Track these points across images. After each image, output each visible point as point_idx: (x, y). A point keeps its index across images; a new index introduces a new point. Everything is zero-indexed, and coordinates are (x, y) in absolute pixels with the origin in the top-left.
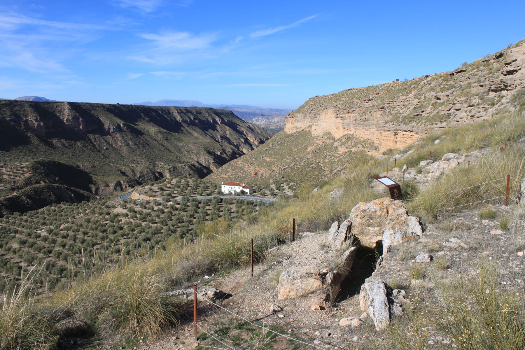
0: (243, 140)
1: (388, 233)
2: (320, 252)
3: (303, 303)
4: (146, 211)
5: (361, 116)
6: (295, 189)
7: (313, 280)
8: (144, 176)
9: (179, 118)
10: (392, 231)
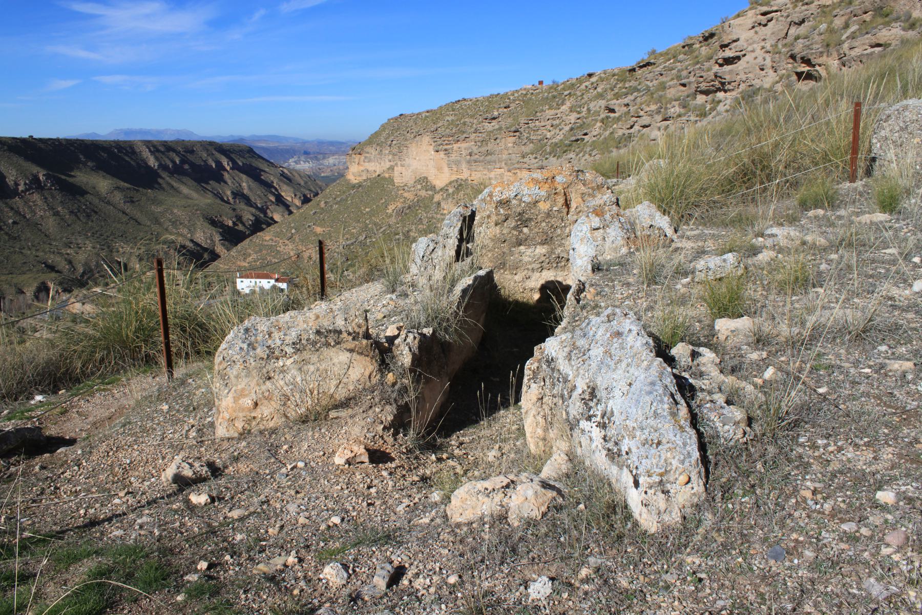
0: (273, 198)
1: (585, 228)
3: (307, 444)
5: (480, 147)
7: (344, 357)
8: (91, 271)
9: (152, 162)
10: (596, 222)
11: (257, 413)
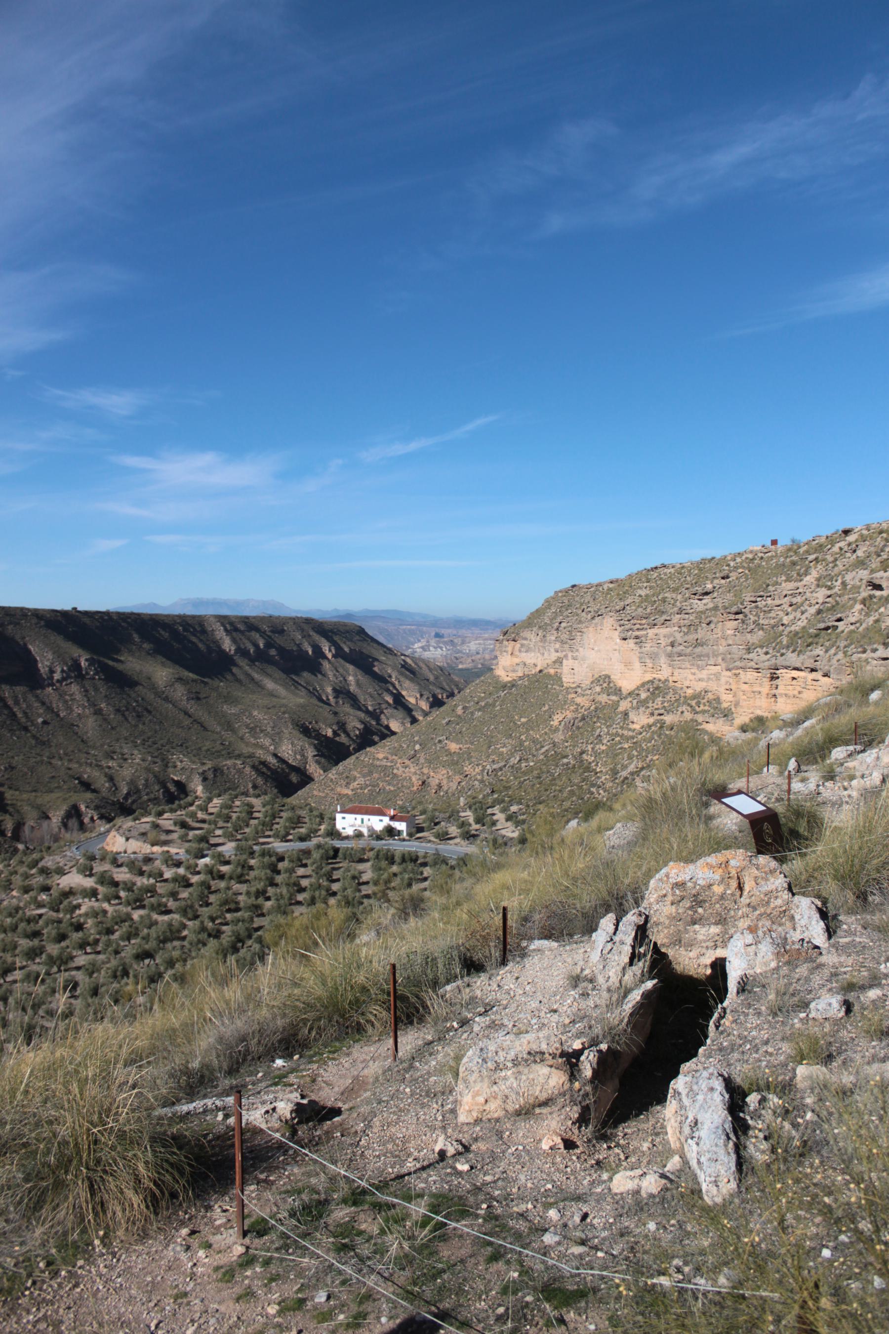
0: (390, 699)
1: (740, 944)
2: (566, 992)
3: (522, 1131)
4: (142, 882)
5: (686, 634)
6: (524, 822)
7: (545, 1070)
8: (138, 791)
9: (228, 645)
10: (749, 938)
11: (487, 1107)
